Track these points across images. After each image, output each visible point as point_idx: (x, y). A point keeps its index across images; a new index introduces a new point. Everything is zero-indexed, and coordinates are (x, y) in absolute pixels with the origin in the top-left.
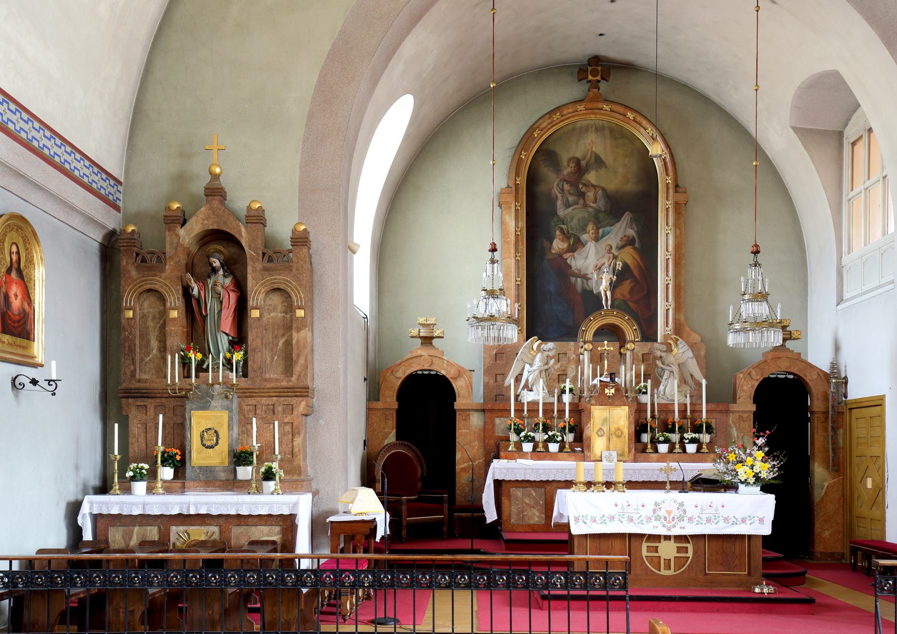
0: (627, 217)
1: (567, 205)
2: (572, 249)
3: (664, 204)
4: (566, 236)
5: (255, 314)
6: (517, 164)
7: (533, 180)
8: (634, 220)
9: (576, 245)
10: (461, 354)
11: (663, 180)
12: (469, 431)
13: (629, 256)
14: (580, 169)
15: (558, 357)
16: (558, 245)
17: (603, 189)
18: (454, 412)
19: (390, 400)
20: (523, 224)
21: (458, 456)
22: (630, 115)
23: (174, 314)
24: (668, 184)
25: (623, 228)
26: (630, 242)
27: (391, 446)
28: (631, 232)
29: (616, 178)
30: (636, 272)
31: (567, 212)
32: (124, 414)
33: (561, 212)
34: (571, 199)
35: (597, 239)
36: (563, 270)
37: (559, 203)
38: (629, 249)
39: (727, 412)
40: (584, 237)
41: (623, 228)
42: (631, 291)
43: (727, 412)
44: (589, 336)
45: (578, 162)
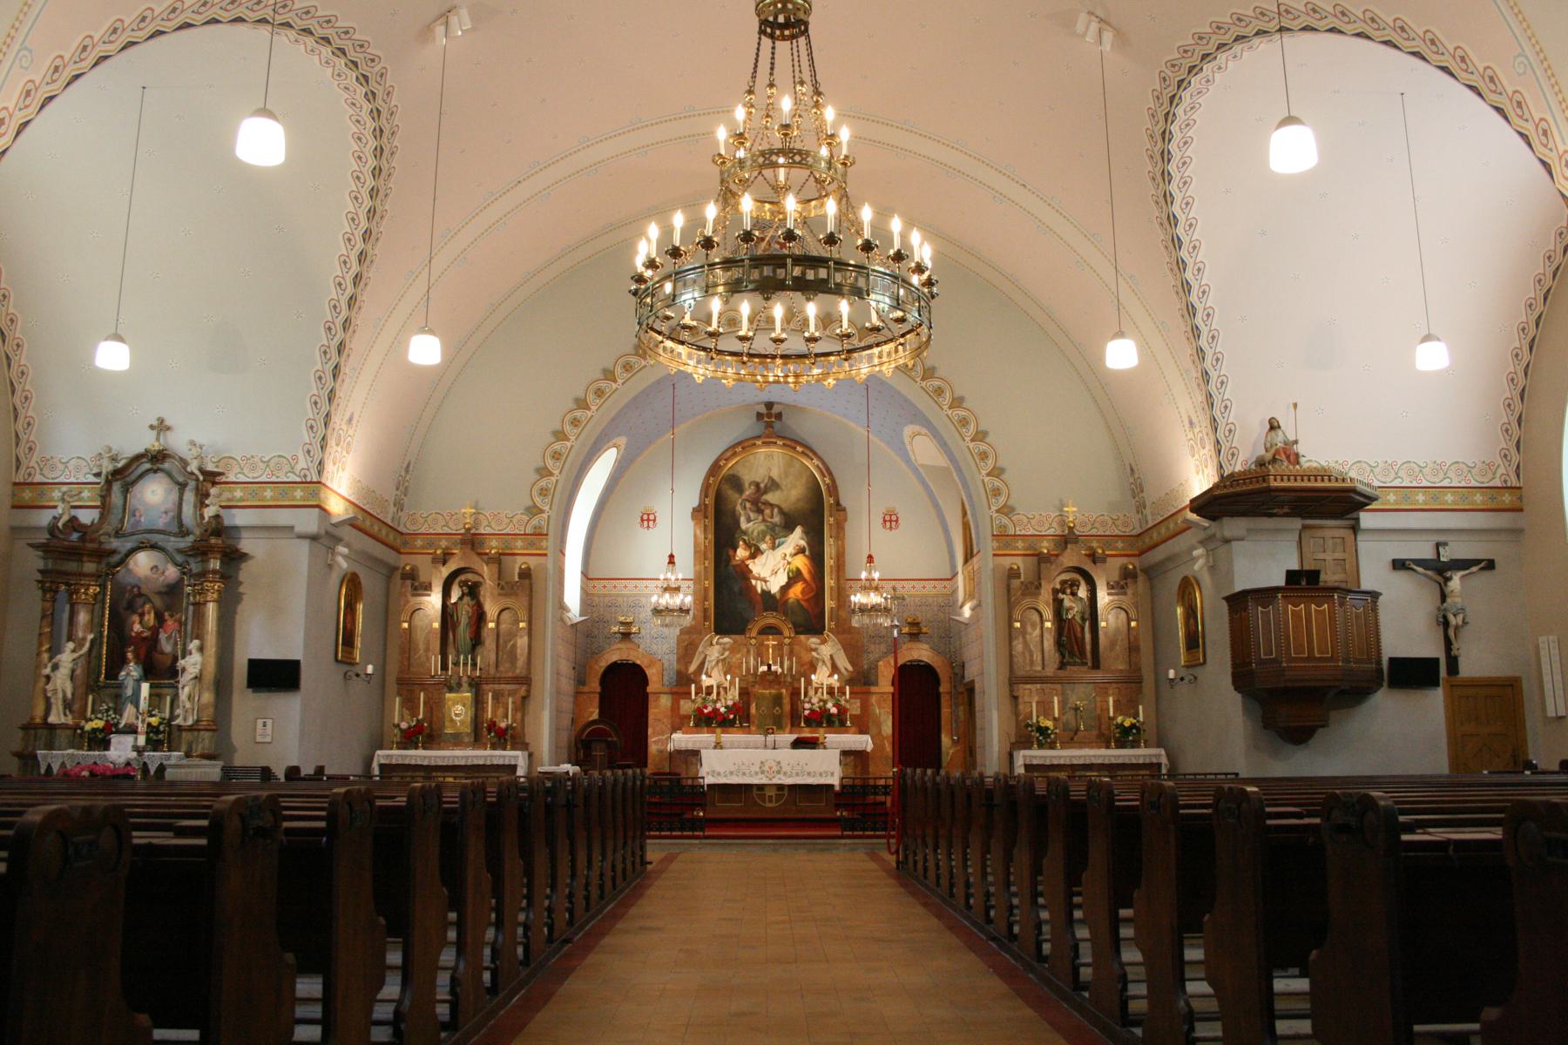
0: (798, 531)
1: (749, 520)
2: (753, 556)
3: (829, 521)
4: (748, 545)
5: (1103, 624)
6: (706, 488)
7: (719, 499)
8: (806, 533)
9: (756, 553)
10: (656, 648)
11: (828, 501)
12: (660, 706)
13: (801, 563)
14: (760, 490)
15: (733, 650)
16: (741, 553)
17: (780, 509)
18: (647, 695)
19: (594, 685)
20: (711, 536)
21: (650, 731)
22: (799, 449)
23: (1048, 624)
24: (706, 589)
25: (797, 538)
26: (801, 551)
27: (594, 722)
28: (803, 543)
29: (790, 495)
30: (806, 575)
31: (750, 524)
32: (85, 773)
33: (744, 525)
34: (752, 515)
35: (774, 548)
36: (744, 573)
37: (743, 519)
38: (800, 556)
39: (869, 693)
40: (763, 546)
41: (797, 538)
42: (803, 592)
43: (869, 693)
44: (754, 634)
45: (757, 485)
